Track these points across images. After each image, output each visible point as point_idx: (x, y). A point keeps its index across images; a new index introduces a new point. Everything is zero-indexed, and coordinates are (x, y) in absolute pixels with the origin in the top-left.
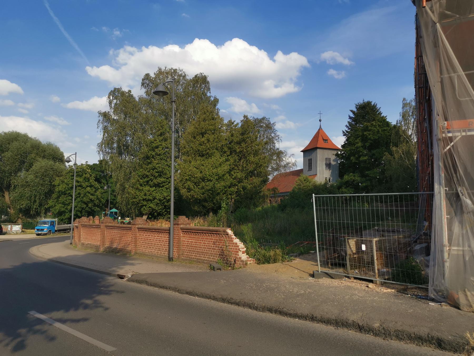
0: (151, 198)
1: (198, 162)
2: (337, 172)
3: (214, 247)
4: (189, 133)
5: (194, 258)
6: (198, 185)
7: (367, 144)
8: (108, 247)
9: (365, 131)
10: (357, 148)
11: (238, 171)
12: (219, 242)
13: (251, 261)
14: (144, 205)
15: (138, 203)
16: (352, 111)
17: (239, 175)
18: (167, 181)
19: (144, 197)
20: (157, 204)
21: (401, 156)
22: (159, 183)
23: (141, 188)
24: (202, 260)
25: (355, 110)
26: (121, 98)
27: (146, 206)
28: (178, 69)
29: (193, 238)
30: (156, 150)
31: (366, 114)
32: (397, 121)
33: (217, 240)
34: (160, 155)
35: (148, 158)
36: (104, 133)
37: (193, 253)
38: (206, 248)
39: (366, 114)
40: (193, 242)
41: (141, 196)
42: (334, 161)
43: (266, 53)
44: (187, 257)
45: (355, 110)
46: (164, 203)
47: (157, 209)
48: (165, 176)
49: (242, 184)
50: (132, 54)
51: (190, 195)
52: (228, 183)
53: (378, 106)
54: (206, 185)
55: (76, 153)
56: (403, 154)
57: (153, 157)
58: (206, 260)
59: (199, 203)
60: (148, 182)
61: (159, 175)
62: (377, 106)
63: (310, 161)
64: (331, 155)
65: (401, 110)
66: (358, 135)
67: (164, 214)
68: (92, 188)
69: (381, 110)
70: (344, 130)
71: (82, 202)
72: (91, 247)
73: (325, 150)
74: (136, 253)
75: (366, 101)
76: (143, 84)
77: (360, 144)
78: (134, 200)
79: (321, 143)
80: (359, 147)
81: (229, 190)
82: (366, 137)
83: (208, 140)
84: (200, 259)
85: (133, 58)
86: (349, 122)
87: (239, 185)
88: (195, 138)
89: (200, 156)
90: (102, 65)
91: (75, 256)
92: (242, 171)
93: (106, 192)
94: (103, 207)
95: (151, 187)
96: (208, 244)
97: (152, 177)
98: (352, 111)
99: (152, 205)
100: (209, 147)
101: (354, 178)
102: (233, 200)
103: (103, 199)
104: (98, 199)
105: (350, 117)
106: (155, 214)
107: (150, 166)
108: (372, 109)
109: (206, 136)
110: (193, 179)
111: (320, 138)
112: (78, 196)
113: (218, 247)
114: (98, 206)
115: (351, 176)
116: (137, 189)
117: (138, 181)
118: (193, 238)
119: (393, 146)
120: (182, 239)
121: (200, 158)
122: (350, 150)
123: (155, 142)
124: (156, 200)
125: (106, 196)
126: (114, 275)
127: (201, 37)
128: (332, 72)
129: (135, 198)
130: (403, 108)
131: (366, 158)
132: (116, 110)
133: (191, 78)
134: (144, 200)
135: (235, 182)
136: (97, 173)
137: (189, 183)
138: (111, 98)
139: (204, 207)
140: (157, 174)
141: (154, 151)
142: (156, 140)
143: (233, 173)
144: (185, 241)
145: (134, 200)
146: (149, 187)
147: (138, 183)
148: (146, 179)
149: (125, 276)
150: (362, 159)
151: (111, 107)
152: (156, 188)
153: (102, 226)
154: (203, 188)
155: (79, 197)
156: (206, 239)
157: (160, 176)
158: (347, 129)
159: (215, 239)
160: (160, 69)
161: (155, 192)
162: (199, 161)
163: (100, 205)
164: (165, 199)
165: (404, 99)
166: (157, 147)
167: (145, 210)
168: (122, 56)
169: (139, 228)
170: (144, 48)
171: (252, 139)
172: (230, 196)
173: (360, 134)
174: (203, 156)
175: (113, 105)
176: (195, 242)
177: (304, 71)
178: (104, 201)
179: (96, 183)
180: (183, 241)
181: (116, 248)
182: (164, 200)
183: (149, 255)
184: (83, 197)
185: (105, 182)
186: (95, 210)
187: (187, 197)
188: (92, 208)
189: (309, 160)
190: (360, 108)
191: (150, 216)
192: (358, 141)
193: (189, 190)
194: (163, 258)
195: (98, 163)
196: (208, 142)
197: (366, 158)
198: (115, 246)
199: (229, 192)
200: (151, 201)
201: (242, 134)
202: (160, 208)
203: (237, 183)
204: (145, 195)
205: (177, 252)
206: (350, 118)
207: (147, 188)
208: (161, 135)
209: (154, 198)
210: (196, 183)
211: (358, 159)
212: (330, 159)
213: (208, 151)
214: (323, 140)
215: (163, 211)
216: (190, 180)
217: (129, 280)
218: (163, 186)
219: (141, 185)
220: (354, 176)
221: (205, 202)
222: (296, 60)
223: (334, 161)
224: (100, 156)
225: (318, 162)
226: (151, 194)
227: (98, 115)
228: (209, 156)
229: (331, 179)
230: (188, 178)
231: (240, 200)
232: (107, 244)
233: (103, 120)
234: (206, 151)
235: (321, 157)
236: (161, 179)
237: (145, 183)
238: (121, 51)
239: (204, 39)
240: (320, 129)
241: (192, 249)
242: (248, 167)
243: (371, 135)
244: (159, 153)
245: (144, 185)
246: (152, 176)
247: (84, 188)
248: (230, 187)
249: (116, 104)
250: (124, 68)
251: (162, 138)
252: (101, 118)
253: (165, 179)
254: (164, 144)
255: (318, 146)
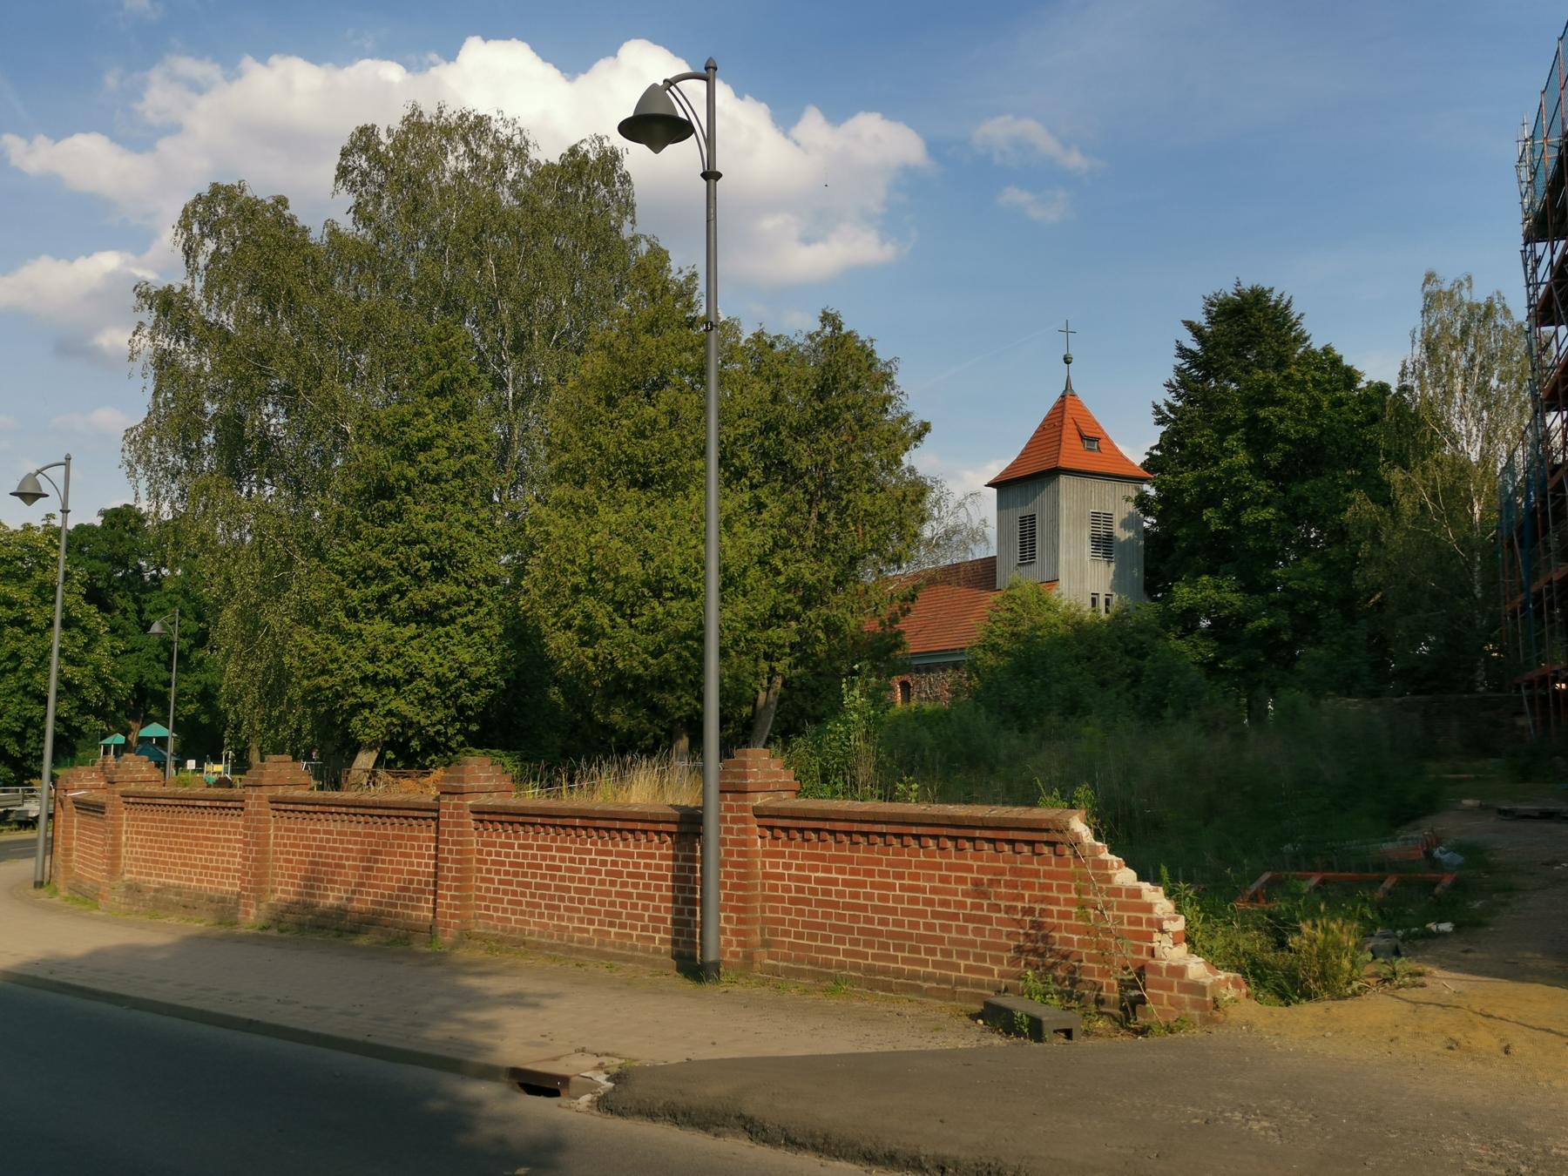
0: (399, 673)
1: (629, 511)
2: (1137, 573)
3: (975, 906)
4: (585, 384)
5: (841, 965)
6: (633, 615)
7: (1273, 459)
8: (289, 908)
9: (1262, 405)
10: (1230, 472)
11: (799, 555)
12: (1009, 885)
13: (1225, 984)
14: (363, 705)
15: (338, 696)
16: (1190, 325)
17: (808, 571)
18: (470, 598)
19: (370, 668)
20: (426, 701)
21: (1423, 507)
22: (436, 606)
23: (353, 627)
24: (899, 973)
25: (1201, 319)
26: (240, 230)
27: (372, 706)
28: (494, 116)
29: (834, 859)
30: (421, 457)
31: (1245, 334)
32: (1404, 367)
33: (1002, 872)
34: (436, 480)
35: (384, 491)
36: (159, 379)
37: (841, 941)
38: (923, 914)
39: (1245, 334)
40: (834, 882)
41: (353, 662)
42: (1125, 524)
43: (764, 106)
44: (799, 960)
45: (1201, 319)
46: (456, 695)
47: (423, 722)
48: (460, 575)
49: (824, 610)
50: (198, 88)
51: (595, 659)
52: (763, 608)
53: (1295, 310)
54: (669, 614)
55: (68, 459)
56: (1434, 497)
57: (408, 490)
58: (928, 977)
59: (632, 694)
60: (383, 599)
61: (434, 568)
62: (1292, 309)
63: (1028, 523)
64: (1117, 503)
65: (1417, 322)
66: (1228, 420)
67: (453, 744)
68: (75, 631)
69: (1307, 326)
70: (1161, 403)
71: (26, 694)
72: (188, 904)
73: (1089, 481)
74: (466, 937)
75: (1246, 286)
76: (343, 172)
77: (1242, 458)
78: (321, 681)
79: (1072, 453)
80: (1241, 468)
81: (763, 636)
82: (1268, 431)
83: (674, 416)
84: (885, 971)
85: (203, 104)
86: (1179, 370)
87: (811, 614)
88: (611, 402)
89: (633, 483)
90: (70, 133)
91: (136, 952)
92: (819, 553)
93: (133, 650)
94: (121, 714)
95: (396, 622)
96: (934, 890)
97: (405, 579)
98: (1190, 325)
99: (399, 704)
100: (677, 443)
101: (1217, 597)
102: (779, 681)
103: (120, 677)
104: (99, 679)
105: (1180, 348)
106: (414, 743)
107: (393, 527)
108: (1272, 321)
109: (667, 394)
110: (610, 586)
111: (1069, 433)
112: (10, 665)
113: (1009, 909)
114: (99, 712)
115: (1204, 588)
116: (336, 629)
117: (341, 594)
118: (834, 859)
119: (1392, 467)
120: (762, 865)
121: (634, 493)
122: (1199, 481)
123: (418, 423)
124: (419, 682)
125: (133, 669)
126: (488, 1073)
127: (493, 31)
128: (1015, 196)
129: (323, 672)
130: (1426, 310)
131: (1268, 513)
132: (220, 277)
133: (556, 161)
134: (364, 680)
135: (791, 600)
136: (97, 564)
137: (589, 603)
138: (196, 230)
139: (655, 710)
140: (428, 564)
141: (413, 462)
142: (424, 415)
143: (780, 564)
144: (781, 877)
145: (321, 681)
146: (387, 624)
147: (338, 602)
148: (375, 589)
149: (565, 1080)
150: (1248, 517)
151: (193, 271)
152: (418, 624)
153: (256, 800)
154: (654, 627)
155: (15, 670)
156: (920, 865)
157: (439, 573)
158: (1170, 398)
159: (981, 870)
160: (416, 112)
161: (414, 643)
162: (632, 506)
163: (105, 705)
164: (462, 675)
165: (1430, 277)
166: (425, 445)
167: (369, 726)
168: (159, 97)
169: (478, 811)
170: (248, 62)
171: (824, 421)
172: (764, 665)
173: (1241, 415)
174: (645, 486)
175: (202, 260)
176: (846, 883)
177: (908, 181)
178: (123, 688)
179: (93, 609)
180: (766, 876)
181: (341, 912)
182: (462, 682)
183: (553, 947)
184: (30, 673)
185: (132, 606)
186: (85, 728)
187: (580, 666)
188: (69, 718)
189: (1023, 519)
190: (1218, 314)
191: (390, 755)
192: (1231, 441)
193: (589, 634)
194: (644, 961)
195: (98, 521)
196: (671, 425)
197: (1268, 513)
198: (331, 898)
199: (763, 647)
200: (398, 687)
201: (822, 393)
202: (439, 715)
203: (798, 608)
204: (373, 658)
205: (735, 933)
206: (1183, 352)
207: (381, 626)
208: (442, 391)
209: (413, 675)
210: (621, 604)
211: (1232, 516)
212: (1108, 517)
213: (674, 463)
214: (1082, 438)
215: (450, 731)
216: (594, 592)
217: (605, 1104)
218: (452, 620)
219: (352, 614)
220: (1218, 588)
221: (661, 689)
222: (881, 140)
223: (1125, 524)
224: (136, 487)
225: (1063, 531)
226: (399, 655)
227: (133, 299)
228: (676, 487)
229: (1115, 598)
230: (581, 580)
231: (814, 683)
232: (283, 891)
233: (156, 326)
234: (662, 462)
235: (1075, 509)
236: (445, 589)
237: (372, 606)
238: (156, 75)
239: (507, 38)
240: (1067, 397)
241: (826, 915)
242: (846, 540)
243: (1288, 423)
244: (434, 470)
245: (368, 611)
246: (406, 571)
247: (35, 630)
248: (766, 626)
249: (216, 256)
250: (166, 145)
251: (445, 406)
252: (149, 317)
253: (463, 588)
254: (454, 433)
255: (1063, 463)
